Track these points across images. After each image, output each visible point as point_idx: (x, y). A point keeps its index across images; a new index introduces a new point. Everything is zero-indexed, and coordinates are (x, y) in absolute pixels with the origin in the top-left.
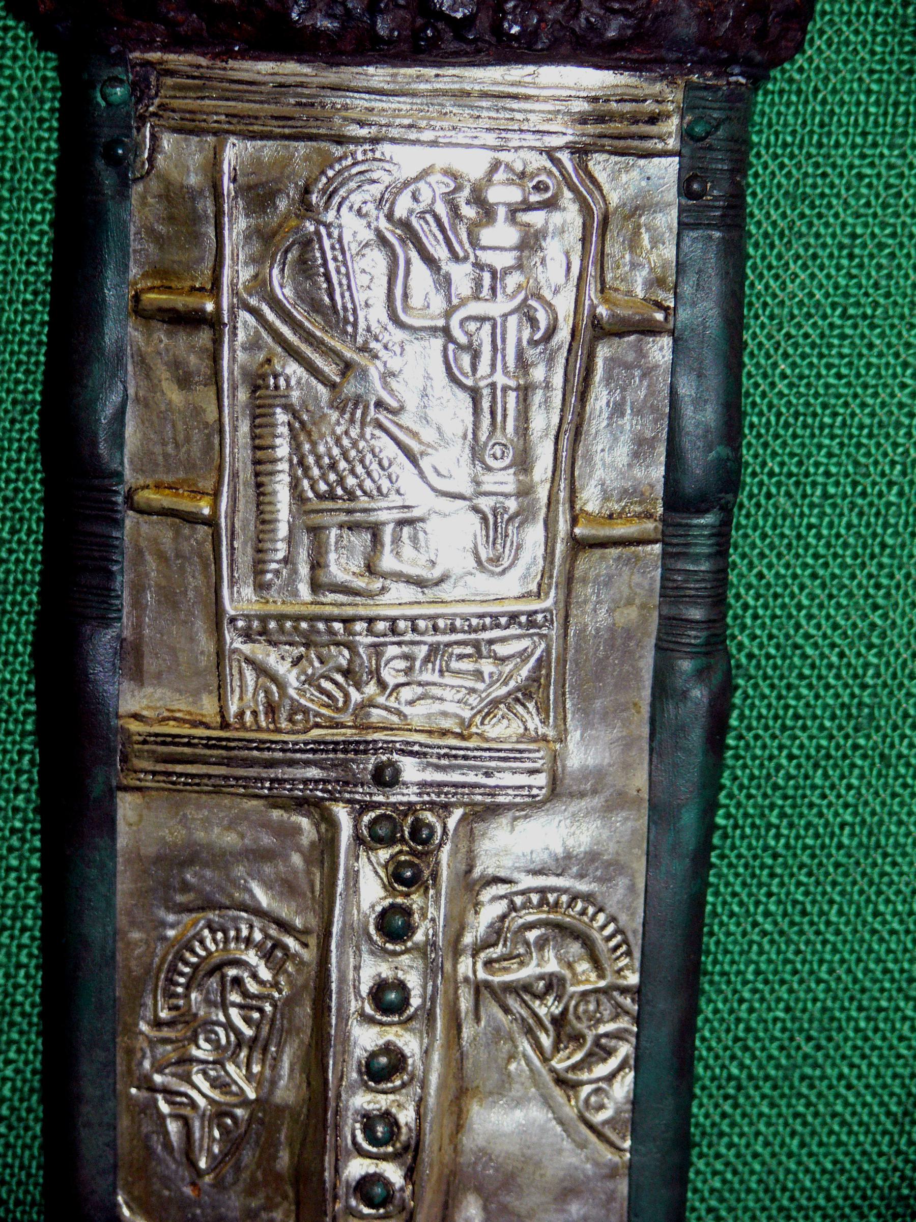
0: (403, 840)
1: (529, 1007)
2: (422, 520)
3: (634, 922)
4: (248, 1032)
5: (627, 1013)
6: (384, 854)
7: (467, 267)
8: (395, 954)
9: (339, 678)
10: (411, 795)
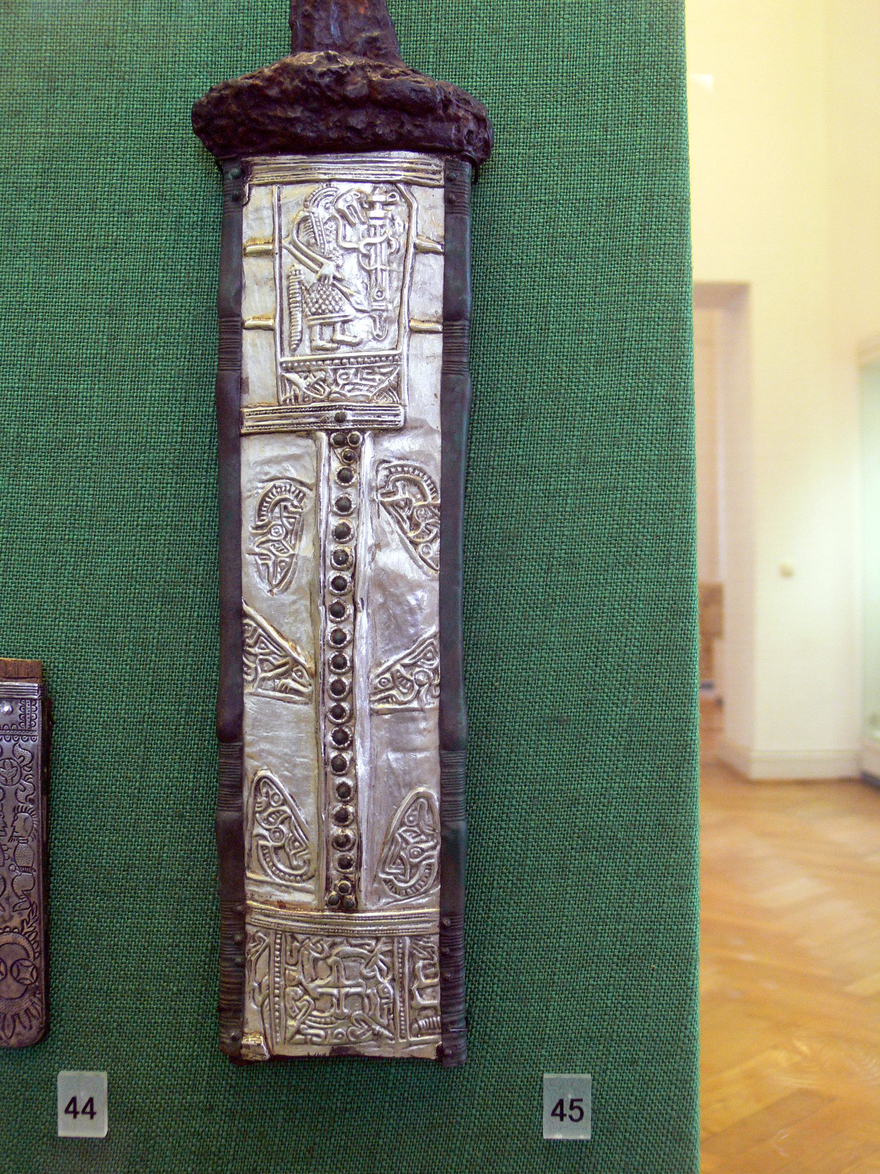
0: (347, 444)
1: (398, 513)
2: (351, 320)
3: (437, 478)
4: (290, 528)
5: (436, 515)
6: (339, 450)
7: (366, 226)
8: (346, 487)
9: (321, 383)
10: (350, 426)
